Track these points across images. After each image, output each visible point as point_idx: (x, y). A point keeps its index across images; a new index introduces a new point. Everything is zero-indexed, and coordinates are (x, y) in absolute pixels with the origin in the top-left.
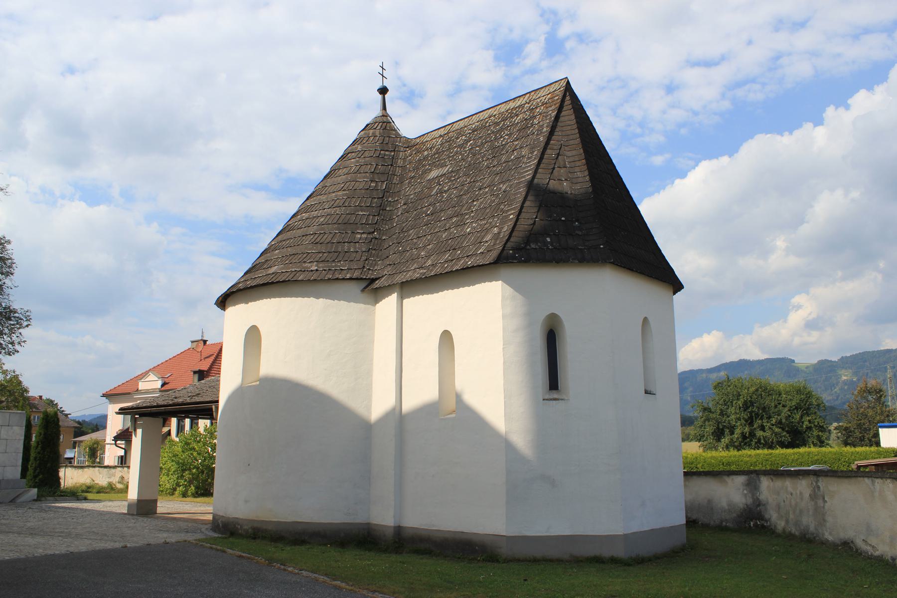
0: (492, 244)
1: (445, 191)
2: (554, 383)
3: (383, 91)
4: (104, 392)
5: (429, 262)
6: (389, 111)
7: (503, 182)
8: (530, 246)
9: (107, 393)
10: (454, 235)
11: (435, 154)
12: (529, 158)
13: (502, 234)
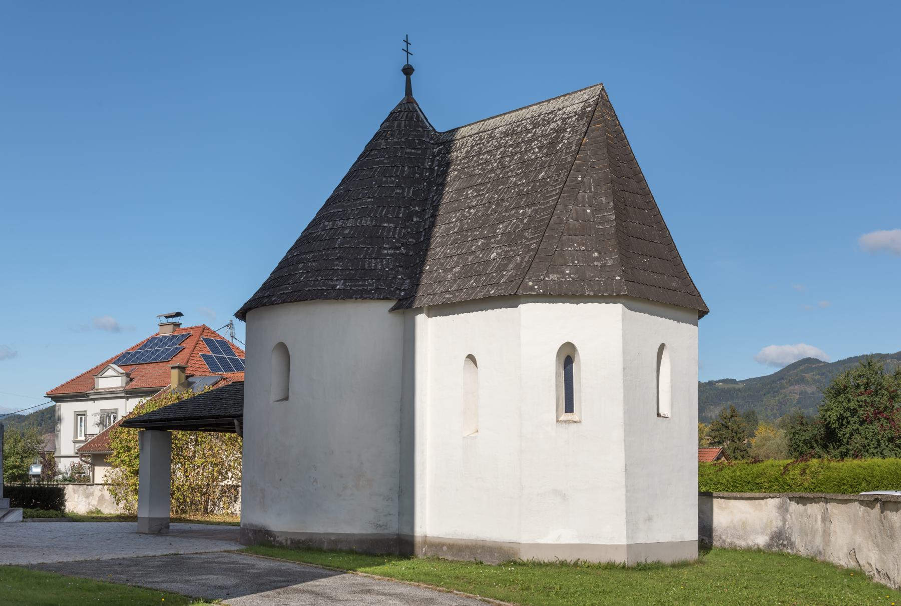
0: (514, 275)
1: (473, 206)
2: (569, 408)
3: (408, 71)
4: (49, 390)
5: (455, 287)
6: (415, 96)
7: (529, 206)
8: (549, 277)
9: (52, 393)
10: (480, 260)
11: (464, 159)
12: (556, 181)
13: (524, 264)
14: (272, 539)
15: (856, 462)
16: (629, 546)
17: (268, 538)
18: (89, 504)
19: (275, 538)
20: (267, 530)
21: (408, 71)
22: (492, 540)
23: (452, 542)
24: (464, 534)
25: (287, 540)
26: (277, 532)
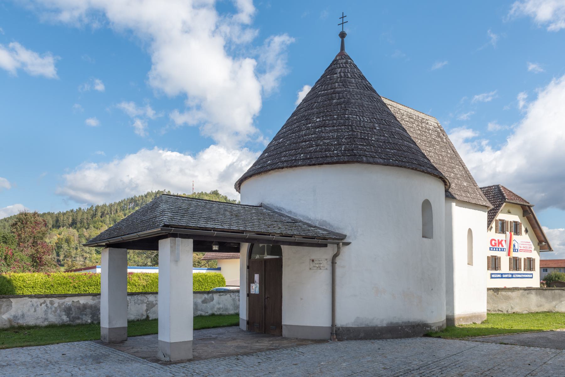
3: (343, 35)
14: (429, 329)
15: (83, 273)
16: (109, 329)
17: (426, 328)
18: (187, 30)
19: (430, 327)
20: (425, 324)
21: (343, 35)
22: (471, 313)
23: (463, 316)
24: (395, 317)
25: (436, 328)
26: (432, 323)
